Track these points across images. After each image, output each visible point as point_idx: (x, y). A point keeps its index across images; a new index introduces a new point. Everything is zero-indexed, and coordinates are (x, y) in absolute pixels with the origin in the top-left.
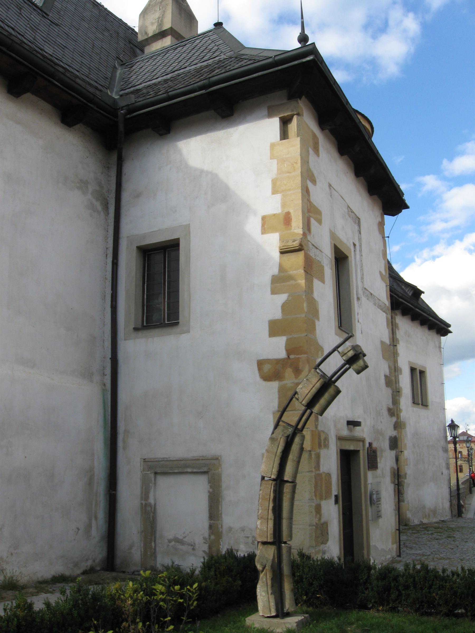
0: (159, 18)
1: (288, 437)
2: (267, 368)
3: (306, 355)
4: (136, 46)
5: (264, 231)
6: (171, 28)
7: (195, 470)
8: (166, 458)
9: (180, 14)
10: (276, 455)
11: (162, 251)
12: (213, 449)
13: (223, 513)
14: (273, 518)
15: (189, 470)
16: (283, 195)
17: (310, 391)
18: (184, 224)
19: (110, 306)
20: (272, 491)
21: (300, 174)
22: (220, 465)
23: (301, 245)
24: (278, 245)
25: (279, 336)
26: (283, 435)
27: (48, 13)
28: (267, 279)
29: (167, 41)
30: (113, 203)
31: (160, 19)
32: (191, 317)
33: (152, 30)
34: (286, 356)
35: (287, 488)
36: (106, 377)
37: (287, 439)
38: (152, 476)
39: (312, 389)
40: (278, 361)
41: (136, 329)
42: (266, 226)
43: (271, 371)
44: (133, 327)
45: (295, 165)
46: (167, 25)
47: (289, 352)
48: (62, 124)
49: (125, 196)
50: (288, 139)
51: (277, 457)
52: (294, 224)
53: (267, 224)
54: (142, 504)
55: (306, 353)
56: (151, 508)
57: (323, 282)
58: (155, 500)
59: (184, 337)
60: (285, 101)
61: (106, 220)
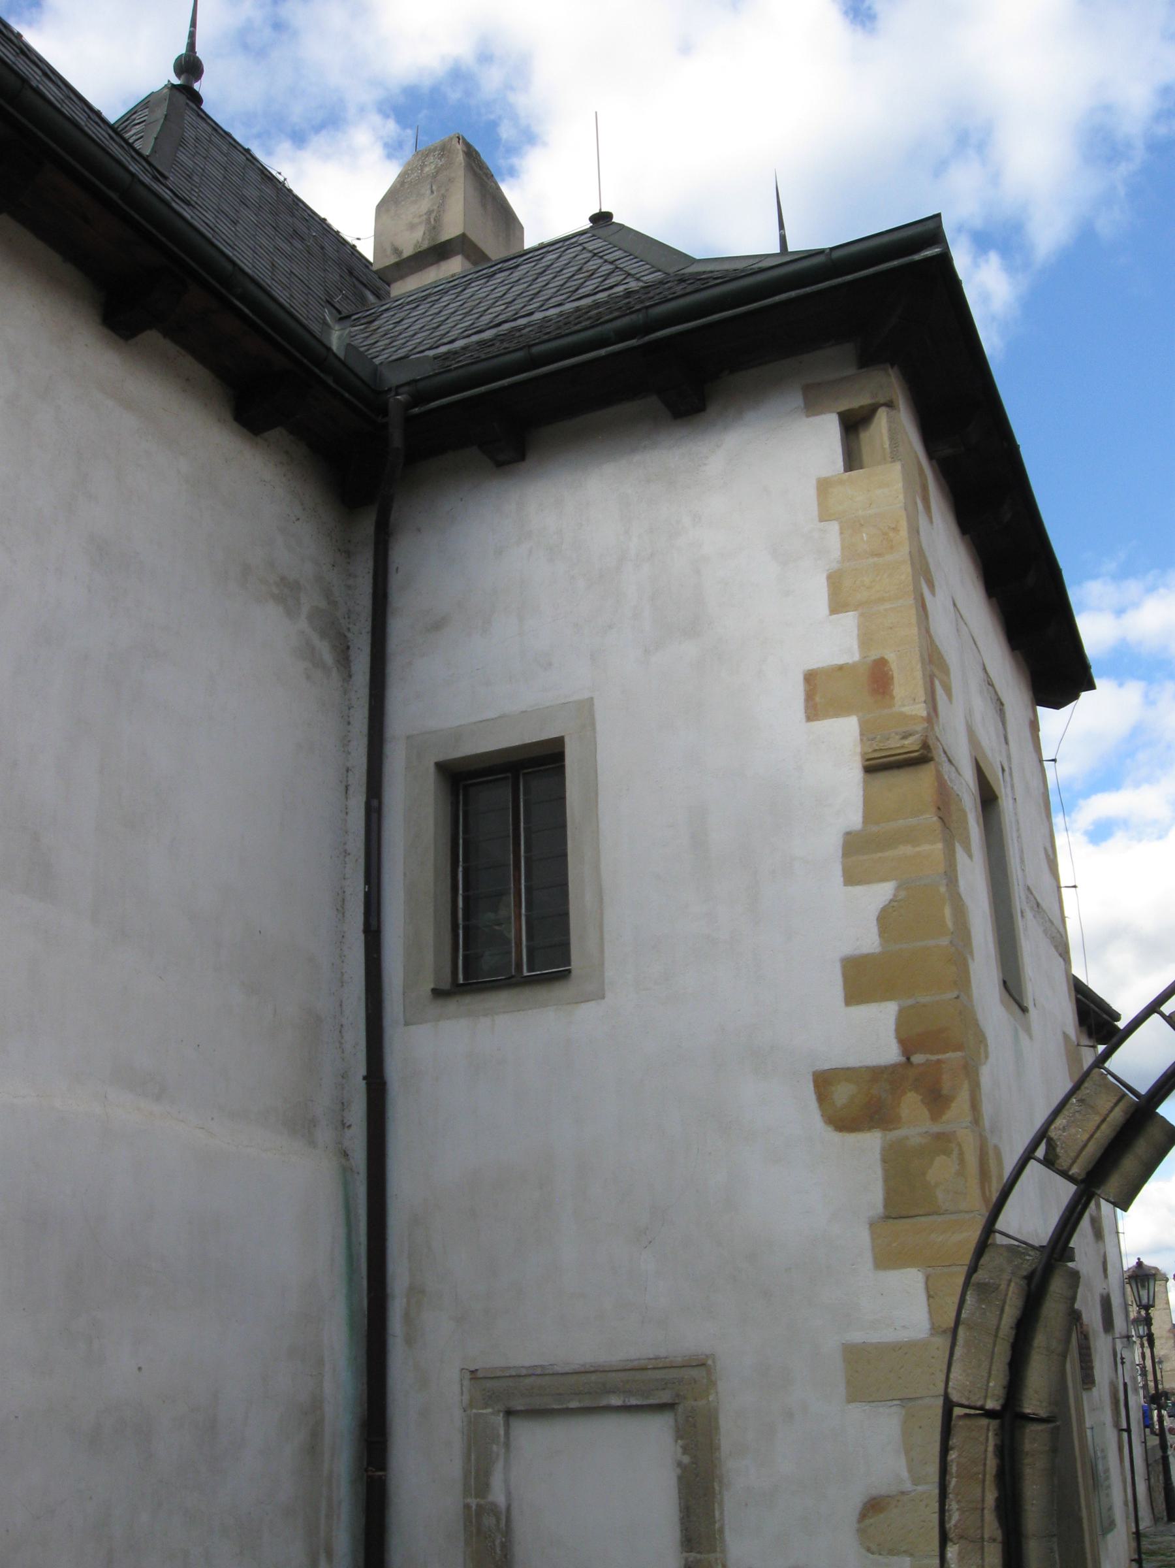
0: (430, 212)
1: (1029, 1278)
2: (842, 1094)
3: (959, 1054)
4: (365, 285)
5: (813, 712)
6: (463, 237)
7: (633, 1401)
8: (542, 1366)
9: (484, 205)
10: (996, 1336)
11: (509, 775)
12: (687, 1337)
13: (727, 1528)
14: (999, 1535)
15: (616, 1401)
16: (862, 615)
17: (1092, 1136)
18: (576, 697)
19: (361, 927)
20: (991, 1448)
21: (908, 557)
22: (712, 1383)
23: (925, 746)
24: (858, 750)
25: (875, 1001)
26: (1013, 1273)
27: (166, 174)
28: (830, 843)
29: (455, 266)
30: (365, 645)
31: (433, 216)
32: (607, 954)
33: (411, 241)
34: (904, 1059)
35: (1034, 1440)
36: (349, 1133)
37: (1029, 1285)
38: (500, 1419)
39: (1098, 1127)
40: (876, 1073)
41: (438, 993)
42: (817, 699)
43: (854, 1102)
44: (432, 986)
45: (891, 534)
46: (452, 229)
47: (908, 1046)
48: (235, 425)
49: (398, 628)
50: (861, 468)
51: (999, 1341)
52: (899, 690)
53: (821, 693)
54: (467, 1507)
55: (959, 1047)
56: (498, 1520)
57: (970, 856)
58: (508, 1494)
59: (587, 1012)
60: (852, 371)
61: (345, 692)
